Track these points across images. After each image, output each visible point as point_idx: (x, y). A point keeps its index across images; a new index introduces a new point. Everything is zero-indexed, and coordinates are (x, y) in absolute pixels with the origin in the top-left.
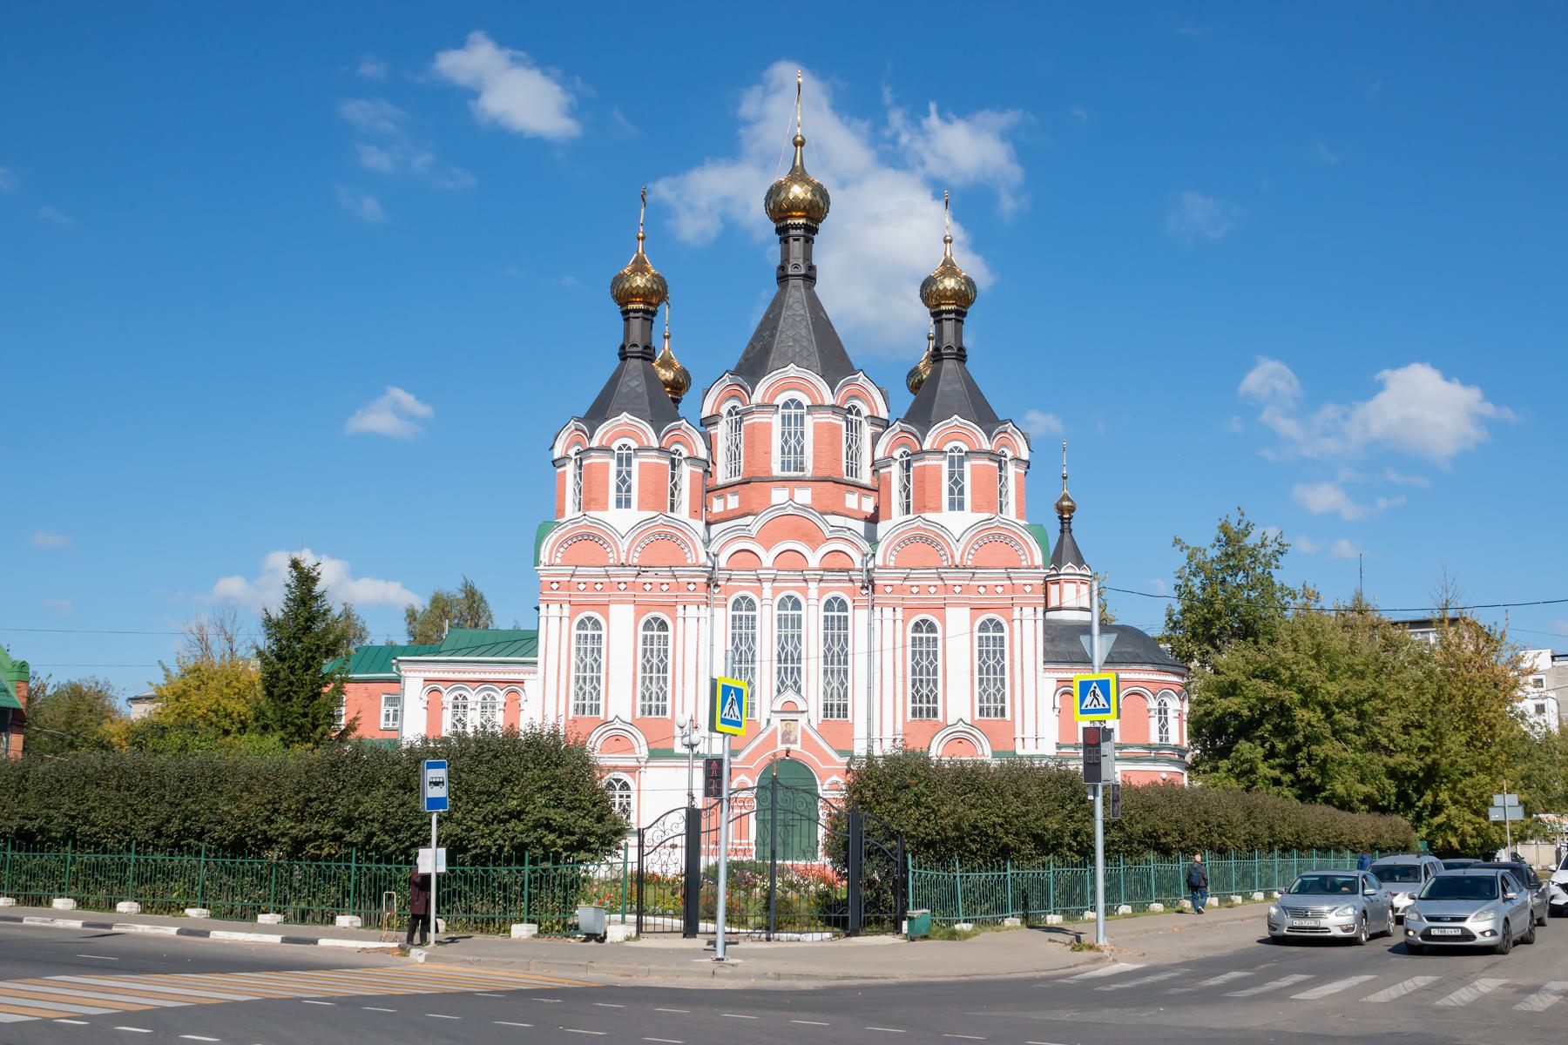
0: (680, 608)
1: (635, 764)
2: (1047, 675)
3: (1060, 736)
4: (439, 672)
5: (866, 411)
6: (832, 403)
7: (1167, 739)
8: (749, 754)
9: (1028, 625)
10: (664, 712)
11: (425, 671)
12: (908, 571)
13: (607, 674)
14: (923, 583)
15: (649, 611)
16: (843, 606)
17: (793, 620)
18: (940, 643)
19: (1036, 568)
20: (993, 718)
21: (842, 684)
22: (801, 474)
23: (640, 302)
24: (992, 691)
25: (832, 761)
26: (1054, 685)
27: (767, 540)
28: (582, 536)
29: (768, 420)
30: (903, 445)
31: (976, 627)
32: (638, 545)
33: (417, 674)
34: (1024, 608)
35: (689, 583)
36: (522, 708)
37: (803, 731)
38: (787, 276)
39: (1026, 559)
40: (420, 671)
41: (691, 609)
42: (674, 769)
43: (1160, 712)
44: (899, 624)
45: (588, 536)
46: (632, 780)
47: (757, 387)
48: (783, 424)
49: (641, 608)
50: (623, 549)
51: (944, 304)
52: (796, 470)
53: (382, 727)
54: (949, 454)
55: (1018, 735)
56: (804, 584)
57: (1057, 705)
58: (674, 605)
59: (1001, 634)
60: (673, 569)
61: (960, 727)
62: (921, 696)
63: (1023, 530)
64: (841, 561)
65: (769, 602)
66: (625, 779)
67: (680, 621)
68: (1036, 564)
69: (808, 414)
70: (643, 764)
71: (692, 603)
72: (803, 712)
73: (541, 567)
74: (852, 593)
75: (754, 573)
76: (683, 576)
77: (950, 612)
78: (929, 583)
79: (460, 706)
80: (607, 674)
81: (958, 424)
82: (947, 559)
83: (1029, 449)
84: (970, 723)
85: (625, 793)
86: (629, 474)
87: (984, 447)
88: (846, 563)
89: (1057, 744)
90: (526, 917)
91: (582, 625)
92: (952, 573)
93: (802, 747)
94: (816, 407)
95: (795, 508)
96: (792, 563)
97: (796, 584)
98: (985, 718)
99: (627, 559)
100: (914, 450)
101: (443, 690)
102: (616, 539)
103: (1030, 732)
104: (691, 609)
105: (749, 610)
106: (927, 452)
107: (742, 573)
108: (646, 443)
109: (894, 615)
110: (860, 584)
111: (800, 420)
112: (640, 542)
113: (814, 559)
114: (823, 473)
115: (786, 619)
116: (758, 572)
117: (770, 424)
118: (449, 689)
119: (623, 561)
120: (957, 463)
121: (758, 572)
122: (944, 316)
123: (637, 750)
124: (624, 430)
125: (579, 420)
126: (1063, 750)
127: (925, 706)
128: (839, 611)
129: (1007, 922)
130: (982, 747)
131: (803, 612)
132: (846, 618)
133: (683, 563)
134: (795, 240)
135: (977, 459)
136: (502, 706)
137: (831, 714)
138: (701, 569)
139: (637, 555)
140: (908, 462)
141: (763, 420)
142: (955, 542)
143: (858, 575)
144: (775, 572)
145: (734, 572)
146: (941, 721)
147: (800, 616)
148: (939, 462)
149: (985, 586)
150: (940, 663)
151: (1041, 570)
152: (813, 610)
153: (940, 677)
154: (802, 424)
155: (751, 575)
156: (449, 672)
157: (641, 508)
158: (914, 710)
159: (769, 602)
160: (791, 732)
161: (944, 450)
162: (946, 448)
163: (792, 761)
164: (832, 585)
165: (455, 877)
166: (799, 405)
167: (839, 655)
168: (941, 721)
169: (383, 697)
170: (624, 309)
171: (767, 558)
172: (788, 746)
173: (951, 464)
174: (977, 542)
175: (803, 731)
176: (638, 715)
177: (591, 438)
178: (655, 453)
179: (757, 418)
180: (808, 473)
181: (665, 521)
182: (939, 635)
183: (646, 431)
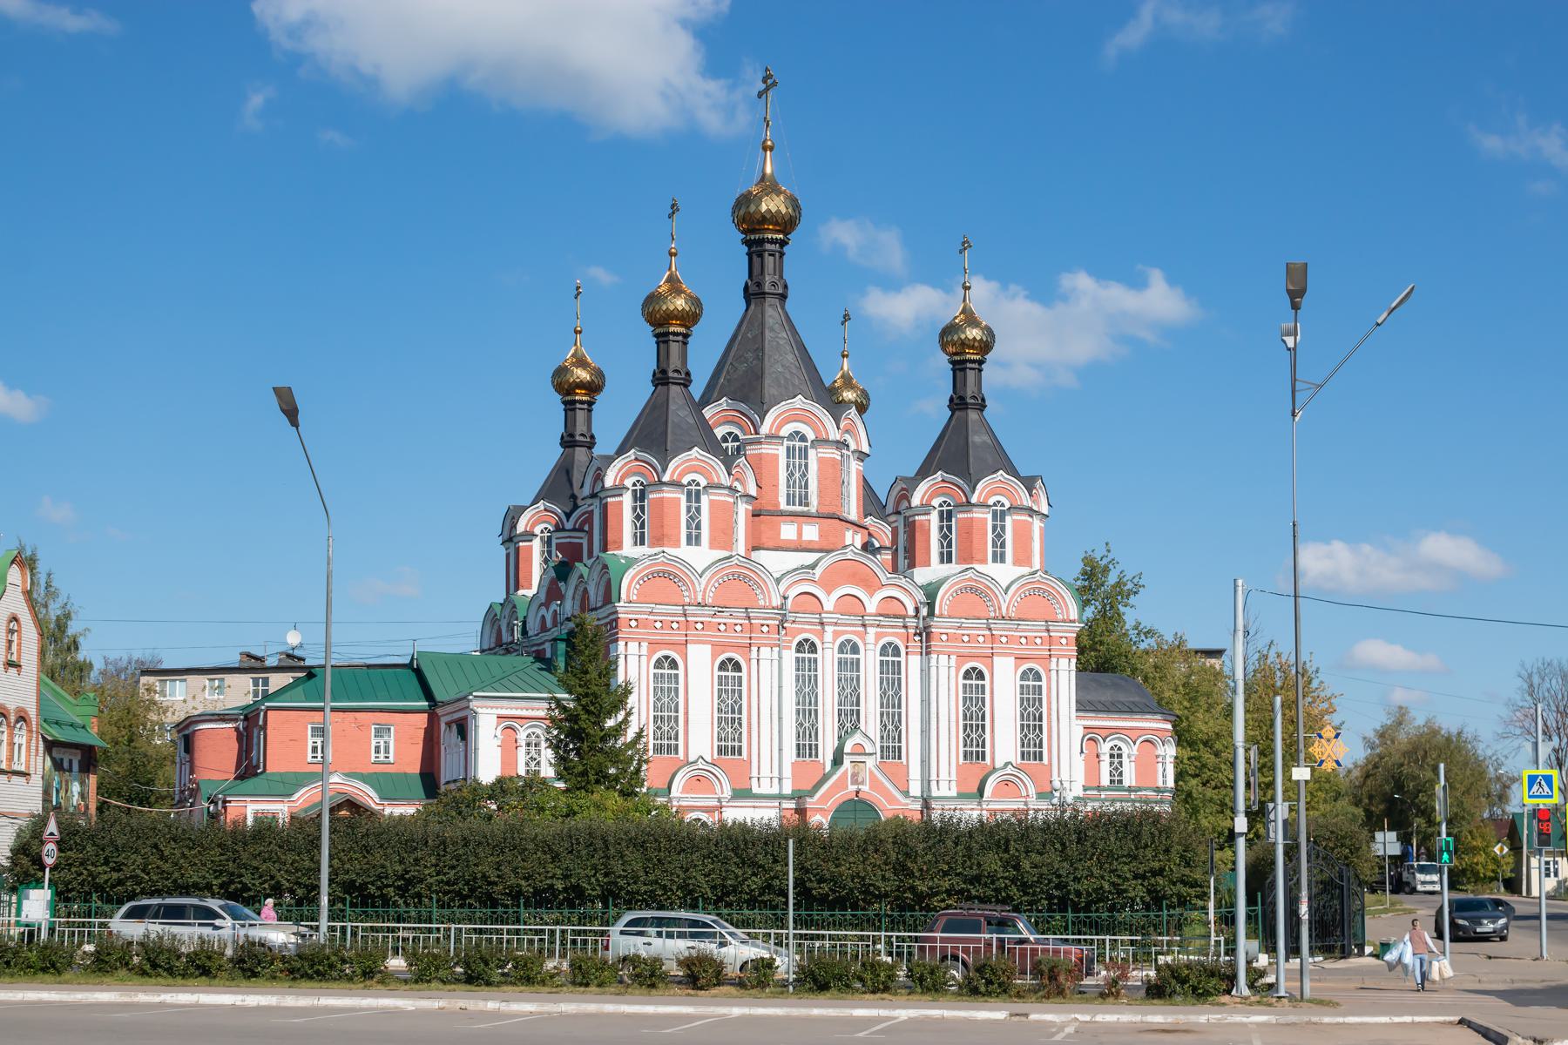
1: (715, 803)
2: (1080, 722)
3: (502, 768)
4: (511, 709)
5: (853, 446)
6: (838, 438)
7: (1120, 782)
8: (823, 795)
9: (1064, 676)
11: (497, 708)
15: (723, 652)
16: (897, 652)
17: (852, 663)
19: (1071, 621)
20: (1032, 762)
22: (806, 509)
24: (807, 725)
26: (1079, 732)
27: (829, 584)
28: (658, 573)
29: (776, 452)
30: (943, 494)
33: (489, 711)
34: (761, 649)
35: (762, 625)
37: (871, 772)
38: (764, 293)
40: (492, 708)
41: (765, 651)
44: (953, 670)
45: (670, 575)
48: (788, 457)
49: (717, 647)
50: (703, 588)
51: (969, 353)
52: (800, 504)
53: (373, 759)
55: (754, 773)
56: (861, 629)
61: (1009, 770)
64: (895, 608)
67: (754, 662)
68: (1072, 618)
69: (812, 447)
71: (766, 645)
72: (871, 754)
73: (622, 604)
76: (757, 618)
80: (686, 713)
87: (1025, 503)
88: (899, 610)
91: (659, 664)
92: (1001, 624)
93: (871, 788)
94: (821, 442)
95: (855, 553)
96: (850, 606)
97: (854, 629)
98: (737, 757)
99: (704, 599)
102: (693, 578)
104: (765, 651)
106: (974, 505)
110: (913, 631)
111: (804, 453)
113: (872, 605)
114: (826, 510)
115: (846, 663)
117: (777, 455)
119: (700, 600)
120: (1000, 516)
122: (969, 365)
124: (695, 465)
126: (1088, 792)
127: (1032, 750)
130: (722, 787)
131: (861, 656)
134: (770, 255)
135: (1017, 514)
138: (776, 611)
140: (950, 513)
141: (770, 451)
147: (858, 660)
148: (985, 516)
151: (1077, 624)
152: (828, 653)
154: (806, 458)
155: (815, 618)
156: (522, 709)
157: (712, 546)
158: (965, 753)
162: (685, 481)
163: (863, 802)
166: (803, 438)
169: (310, 726)
171: (829, 603)
173: (995, 518)
175: (871, 772)
176: (716, 756)
178: (726, 492)
180: (813, 509)
181: (741, 561)
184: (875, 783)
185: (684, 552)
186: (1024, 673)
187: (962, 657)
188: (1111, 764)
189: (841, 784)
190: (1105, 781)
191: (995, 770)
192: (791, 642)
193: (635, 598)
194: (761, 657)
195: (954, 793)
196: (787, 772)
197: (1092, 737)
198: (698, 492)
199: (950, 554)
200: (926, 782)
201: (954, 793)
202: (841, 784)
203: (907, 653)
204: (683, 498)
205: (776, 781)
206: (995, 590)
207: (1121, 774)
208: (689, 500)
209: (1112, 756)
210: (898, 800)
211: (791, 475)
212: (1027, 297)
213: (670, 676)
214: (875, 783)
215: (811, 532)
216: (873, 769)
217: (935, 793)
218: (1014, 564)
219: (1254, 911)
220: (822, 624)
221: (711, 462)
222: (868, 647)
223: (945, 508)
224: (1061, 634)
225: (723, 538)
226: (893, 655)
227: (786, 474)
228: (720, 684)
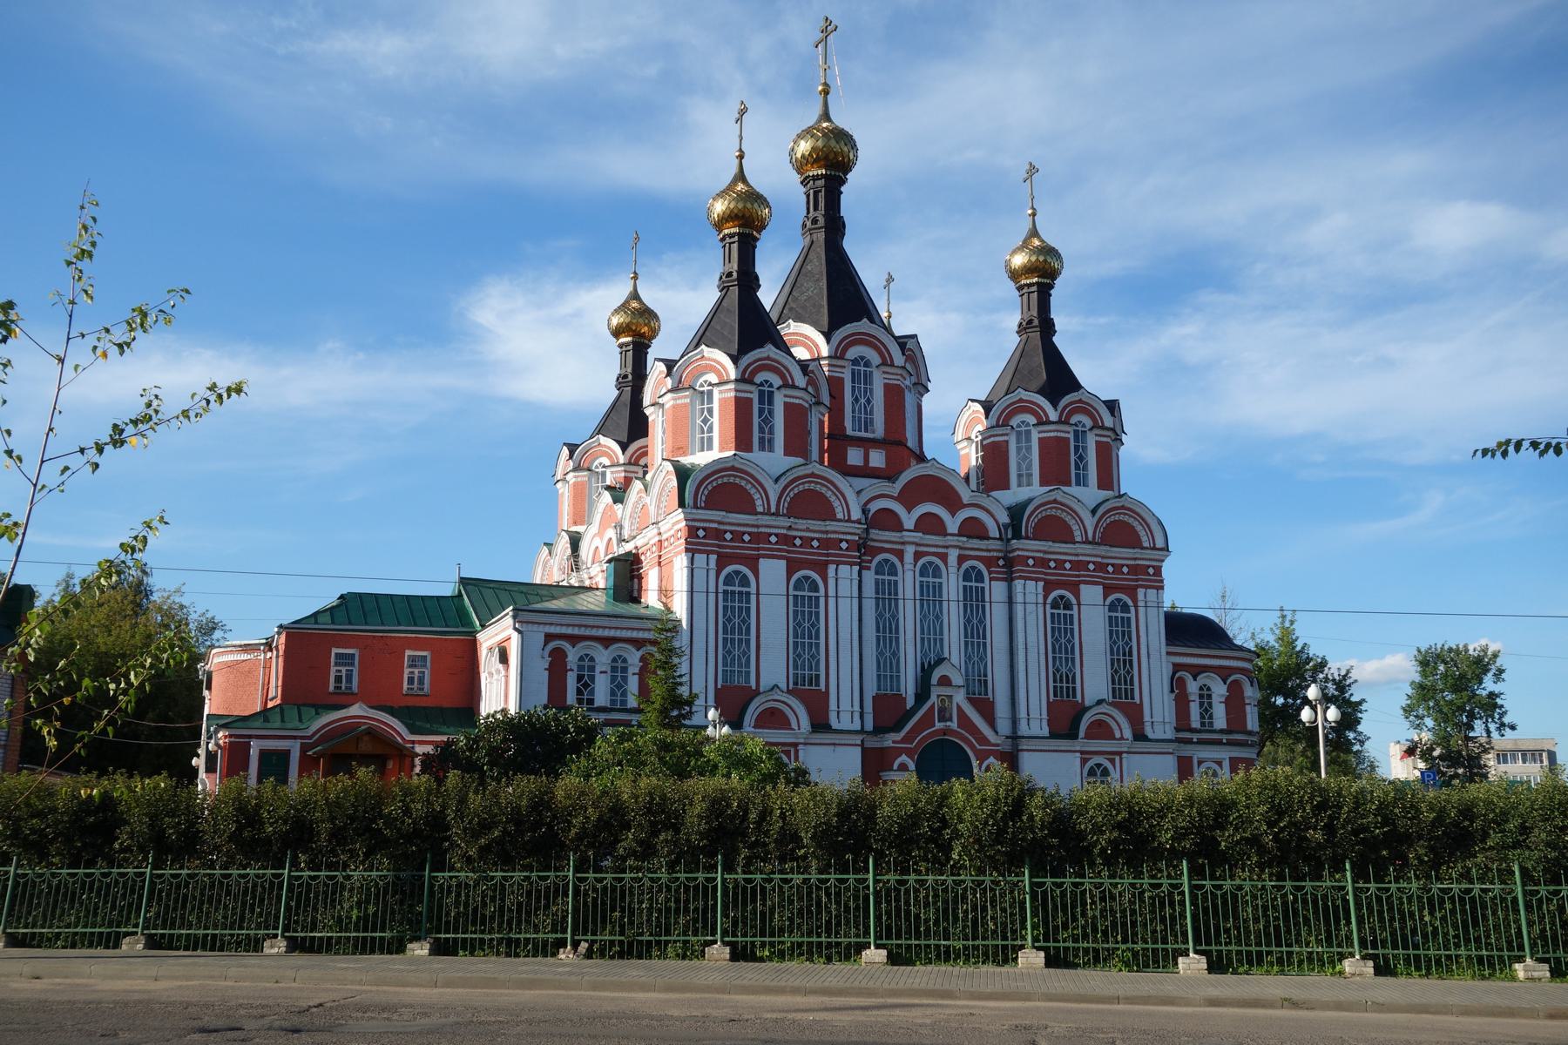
7: (1211, 724)
16: (980, 578)
17: (934, 587)
18: (753, 598)
24: (1122, 672)
42: (832, 747)
43: (614, 669)
44: (712, 574)
48: (853, 381)
49: (1108, 590)
52: (866, 431)
58: (827, 563)
71: (700, 552)
77: (764, 564)
113: (952, 524)
117: (842, 379)
128: (889, 575)
129: (1348, 965)
132: (896, 582)
167: (890, 624)
171: (909, 520)
175: (959, 707)
182: (753, 589)
186: (728, 576)
189: (927, 721)
190: (1195, 724)
192: (870, 562)
193: (703, 505)
194: (840, 575)
200: (1014, 722)
202: (927, 721)
203: (991, 579)
205: (857, 716)
207: (1211, 717)
209: (1201, 696)
211: (856, 400)
213: (740, 593)
215: (877, 459)
217: (1023, 729)
218: (1099, 488)
226: (976, 581)
227: (851, 400)
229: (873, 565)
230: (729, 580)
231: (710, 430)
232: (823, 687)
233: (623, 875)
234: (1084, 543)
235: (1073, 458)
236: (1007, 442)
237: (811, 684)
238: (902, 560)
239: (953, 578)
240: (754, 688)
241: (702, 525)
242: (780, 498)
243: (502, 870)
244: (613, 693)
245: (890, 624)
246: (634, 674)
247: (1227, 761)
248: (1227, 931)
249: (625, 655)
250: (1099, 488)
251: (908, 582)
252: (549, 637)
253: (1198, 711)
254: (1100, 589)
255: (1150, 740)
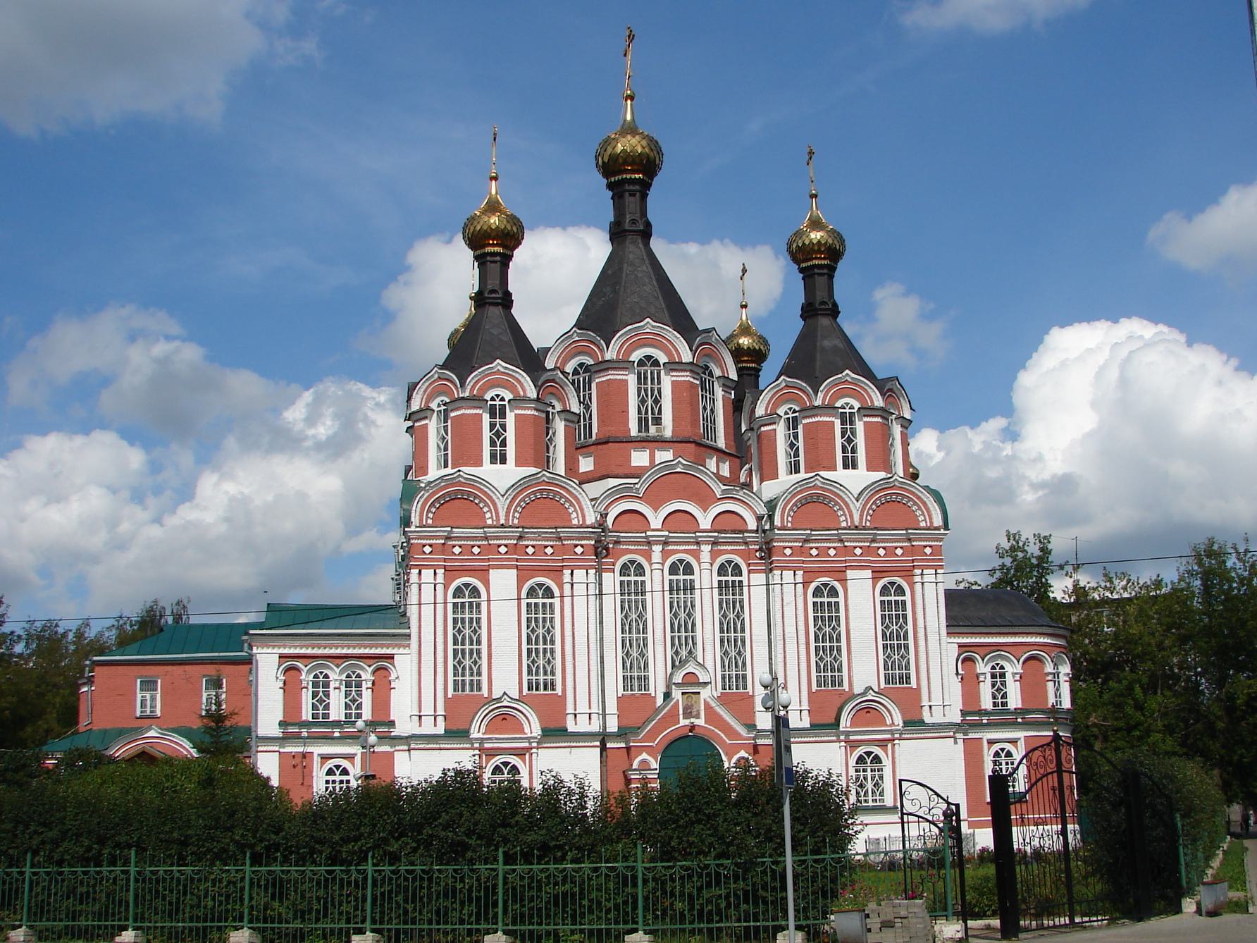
0: (567, 572)
2: (952, 640)
7: (1004, 704)
10: (841, 684)
12: (809, 532)
13: (489, 646)
14: (822, 545)
16: (737, 570)
21: (739, 653)
23: (497, 245)
25: (738, 736)
26: (954, 651)
29: (624, 377)
31: (524, 595)
32: (518, 505)
34: (575, 571)
36: (392, 686)
39: (925, 520)
42: (569, 749)
43: (348, 685)
44: (440, 588)
46: (522, 763)
47: (613, 342)
50: (501, 510)
53: (138, 714)
54: (489, 403)
55: (925, 702)
57: (960, 671)
58: (560, 570)
59: (836, 600)
60: (559, 530)
62: (464, 668)
63: (923, 490)
64: (729, 522)
65: (659, 566)
66: (513, 762)
68: (936, 524)
70: (534, 745)
71: (579, 567)
72: (706, 684)
73: (413, 528)
74: (746, 555)
75: (644, 535)
77: (494, 574)
78: (828, 545)
79: (321, 689)
80: (489, 646)
81: (850, 380)
82: (846, 519)
83: (911, 409)
84: (877, 690)
85: (876, 766)
86: (504, 427)
87: (876, 404)
89: (961, 711)
90: (1240, 888)
93: (706, 722)
94: (674, 366)
98: (905, 685)
99: (507, 519)
100: (804, 406)
101: (302, 667)
102: (494, 497)
103: (937, 700)
105: (637, 575)
107: (630, 535)
108: (522, 393)
109: (435, 579)
112: (520, 501)
113: (705, 521)
116: (648, 533)
118: (308, 667)
121: (648, 533)
123: (527, 730)
125: (444, 367)
130: (891, 716)
133: (569, 525)
134: (630, 195)
136: (370, 685)
137: (737, 685)
138: (590, 530)
139: (517, 515)
142: (855, 502)
143: (753, 537)
144: (666, 533)
145: (622, 535)
146: (847, 690)
149: (884, 548)
150: (524, 631)
153: (525, 647)
154: (659, 383)
157: (870, 468)
159: (659, 566)
160: (692, 705)
161: (485, 398)
162: (488, 397)
164: (678, 547)
165: (383, 880)
166: (656, 363)
167: (735, 624)
168: (847, 690)
169: (139, 681)
170: (479, 252)
172: (692, 720)
174: (874, 503)
176: (525, 691)
177: (463, 385)
179: (612, 376)
181: (548, 477)
182: (841, 599)
183: (522, 380)
184: (711, 715)
185: (487, 471)
186: (884, 587)
187: (450, 573)
188: (315, 695)
190: (307, 714)
191: (854, 696)
195: (440, 730)
196: (612, 707)
197: (967, 657)
198: (503, 407)
199: (797, 464)
201: (440, 730)
203: (749, 572)
204: (837, 422)
206: (844, 496)
207: (1004, 696)
208: (492, 415)
210: (739, 734)
212: (1189, 217)
214: (711, 715)
216: (709, 700)
219: (494, 870)
220: (649, 543)
221: (517, 376)
222: (704, 566)
223: (791, 415)
224: (925, 543)
225: (537, 453)
227: (663, 402)
228: (883, 609)
229: (618, 568)
230: (458, 592)
231: (504, 444)
232: (559, 691)
233: (88, 869)
234: (849, 528)
235: (801, 444)
236: (775, 430)
237: (472, 690)
238: (698, 559)
239: (706, 574)
240: (486, 695)
241: (428, 542)
242: (509, 509)
243: (82, 867)
244: (347, 706)
245: (735, 624)
246: (367, 688)
247: (1023, 739)
248: (421, 899)
249: (326, 671)
250: (868, 470)
251: (656, 579)
252: (282, 657)
253: (310, 701)
254: (868, 573)
255: (928, 725)
